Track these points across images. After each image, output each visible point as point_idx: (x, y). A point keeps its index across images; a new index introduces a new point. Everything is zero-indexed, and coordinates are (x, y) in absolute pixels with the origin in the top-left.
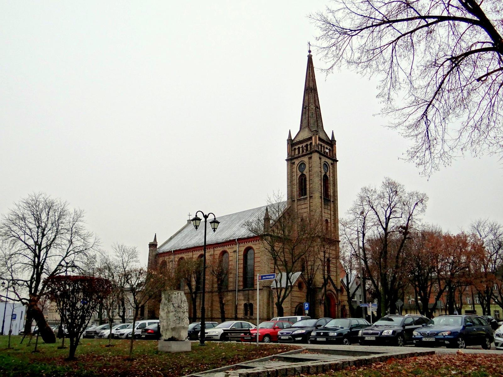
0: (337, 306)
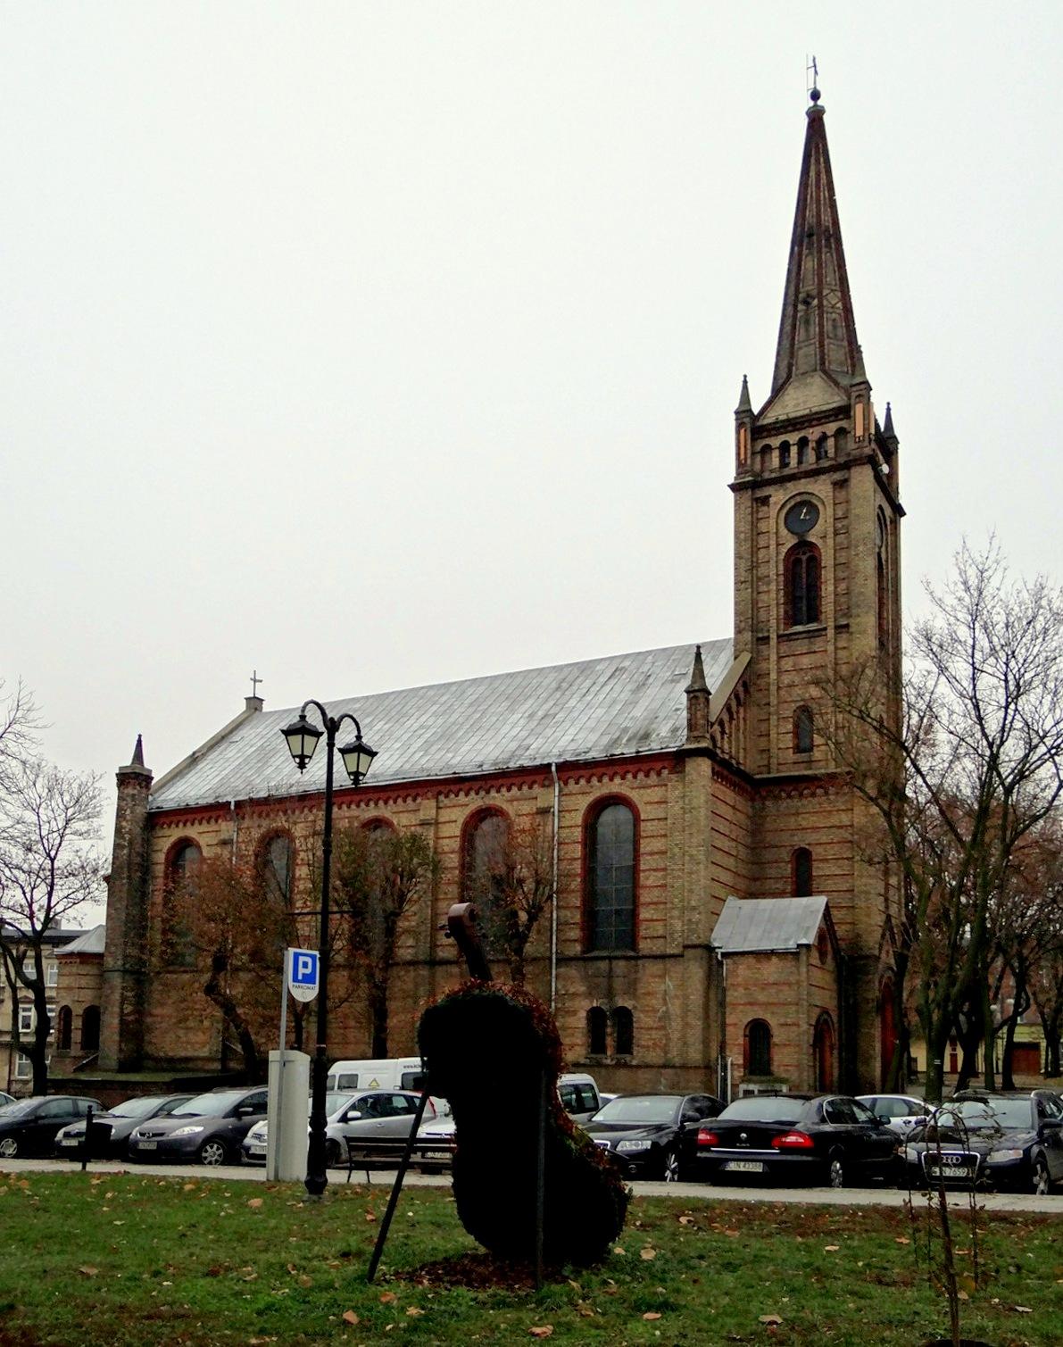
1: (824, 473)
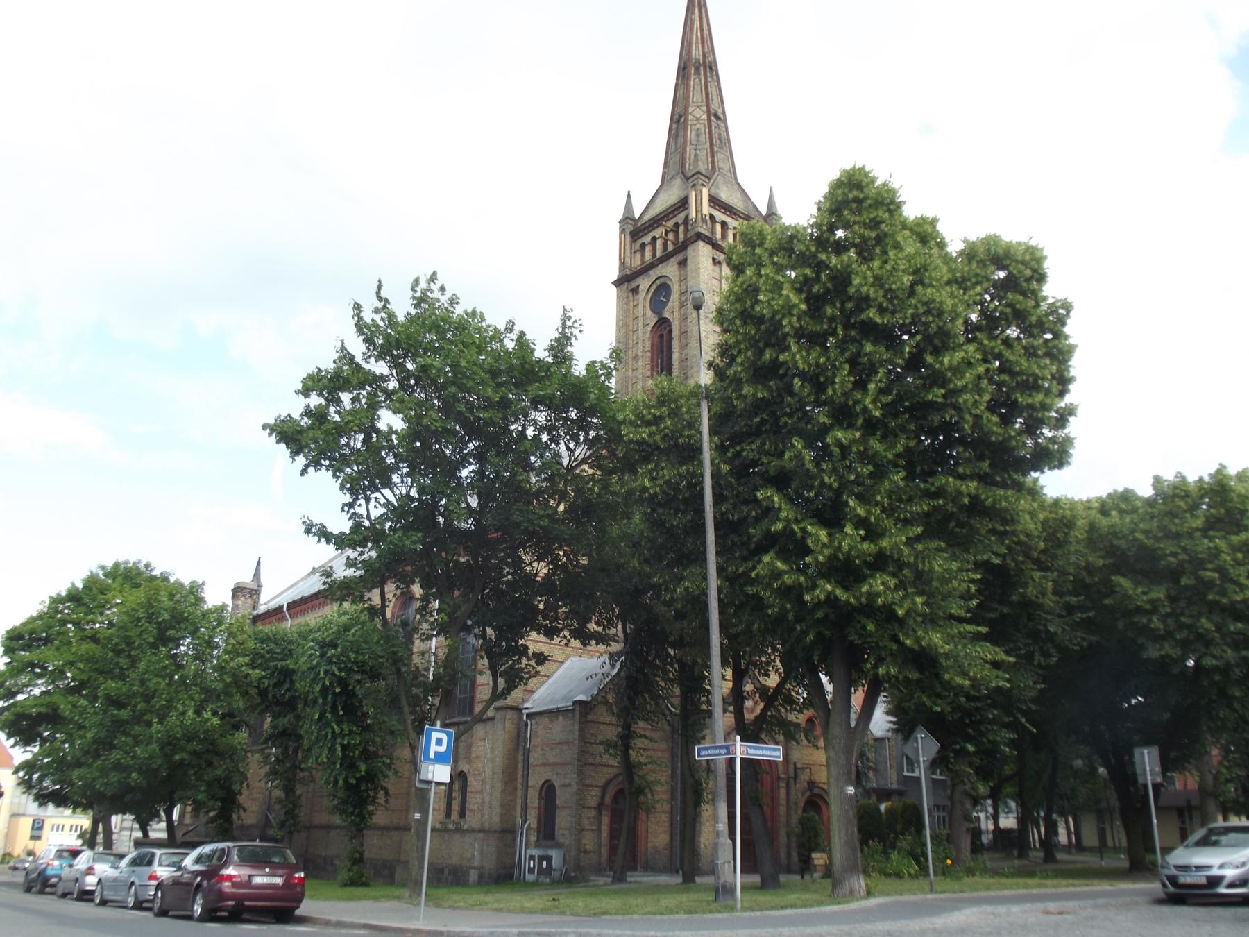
0: (783, 784)
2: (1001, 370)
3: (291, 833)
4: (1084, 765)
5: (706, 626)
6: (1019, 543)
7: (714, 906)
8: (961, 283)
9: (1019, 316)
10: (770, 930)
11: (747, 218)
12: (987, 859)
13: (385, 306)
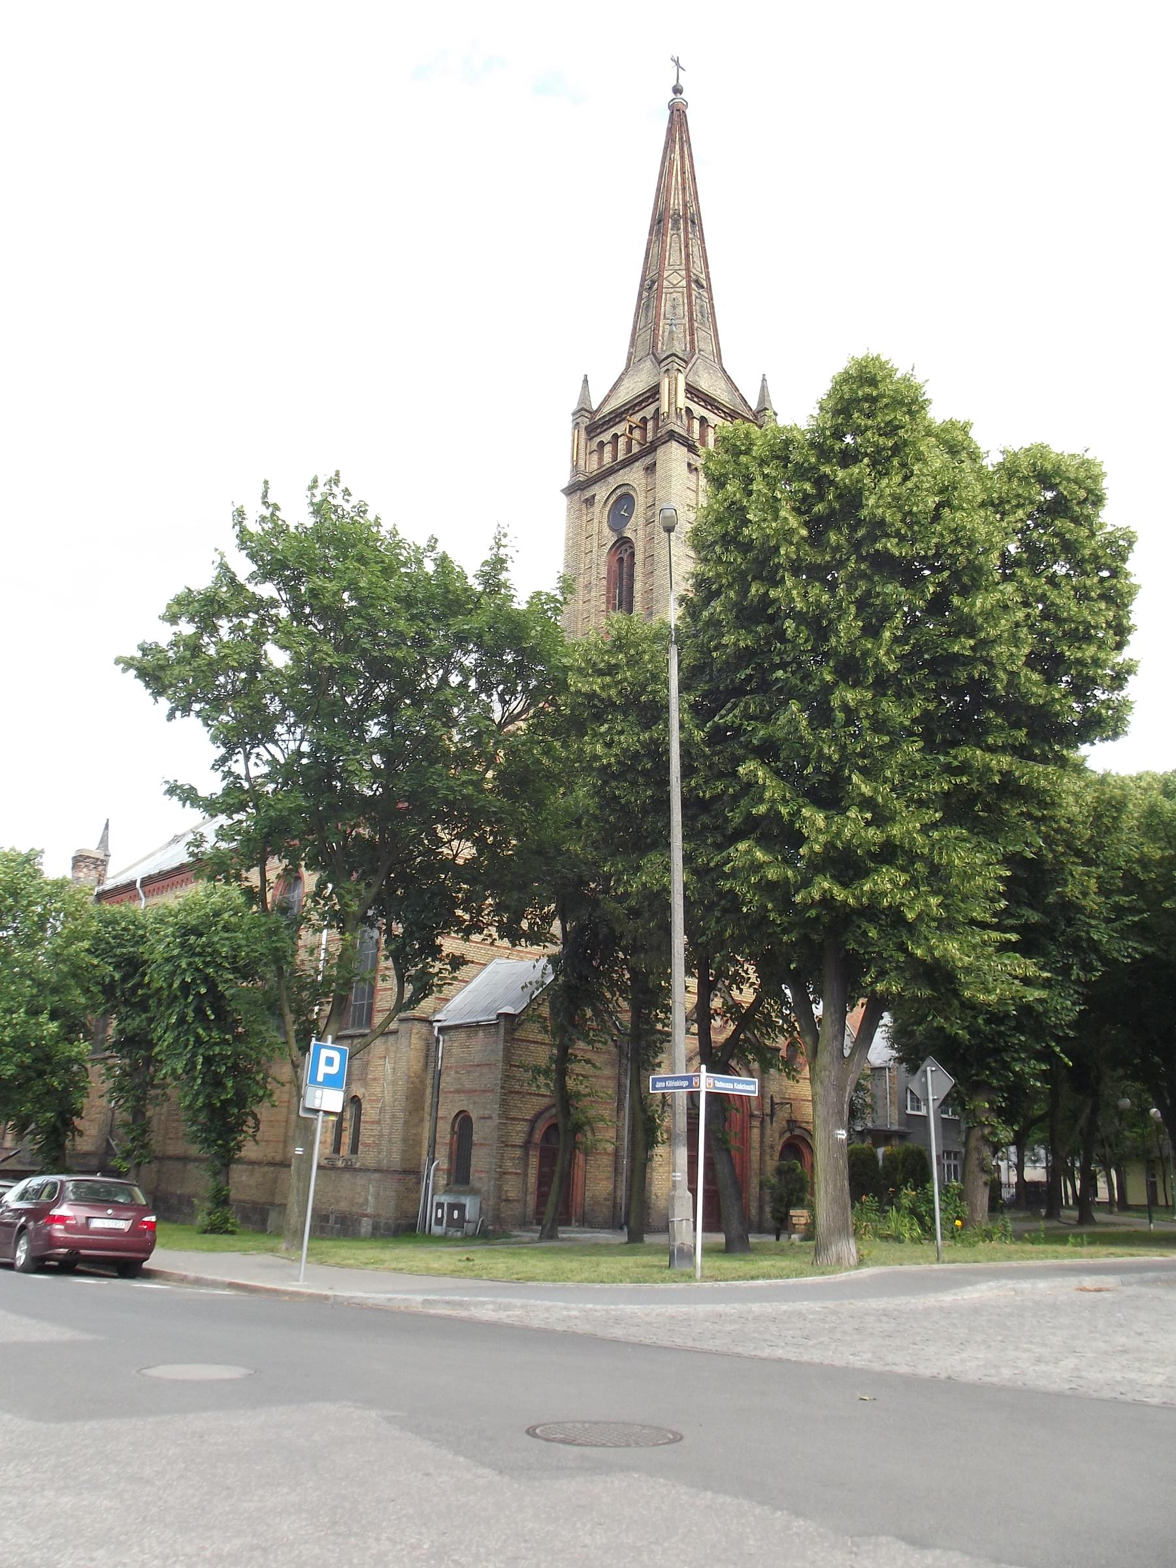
0: (756, 1123)
1: (637, 460)
2: (1045, 616)
3: (139, 1165)
4: (1133, 1103)
5: (667, 929)
6: (1059, 830)
7: (667, 1273)
8: (998, 505)
9: (1069, 548)
10: (736, 1305)
11: (732, 415)
12: (1008, 1220)
13: (273, 514)
